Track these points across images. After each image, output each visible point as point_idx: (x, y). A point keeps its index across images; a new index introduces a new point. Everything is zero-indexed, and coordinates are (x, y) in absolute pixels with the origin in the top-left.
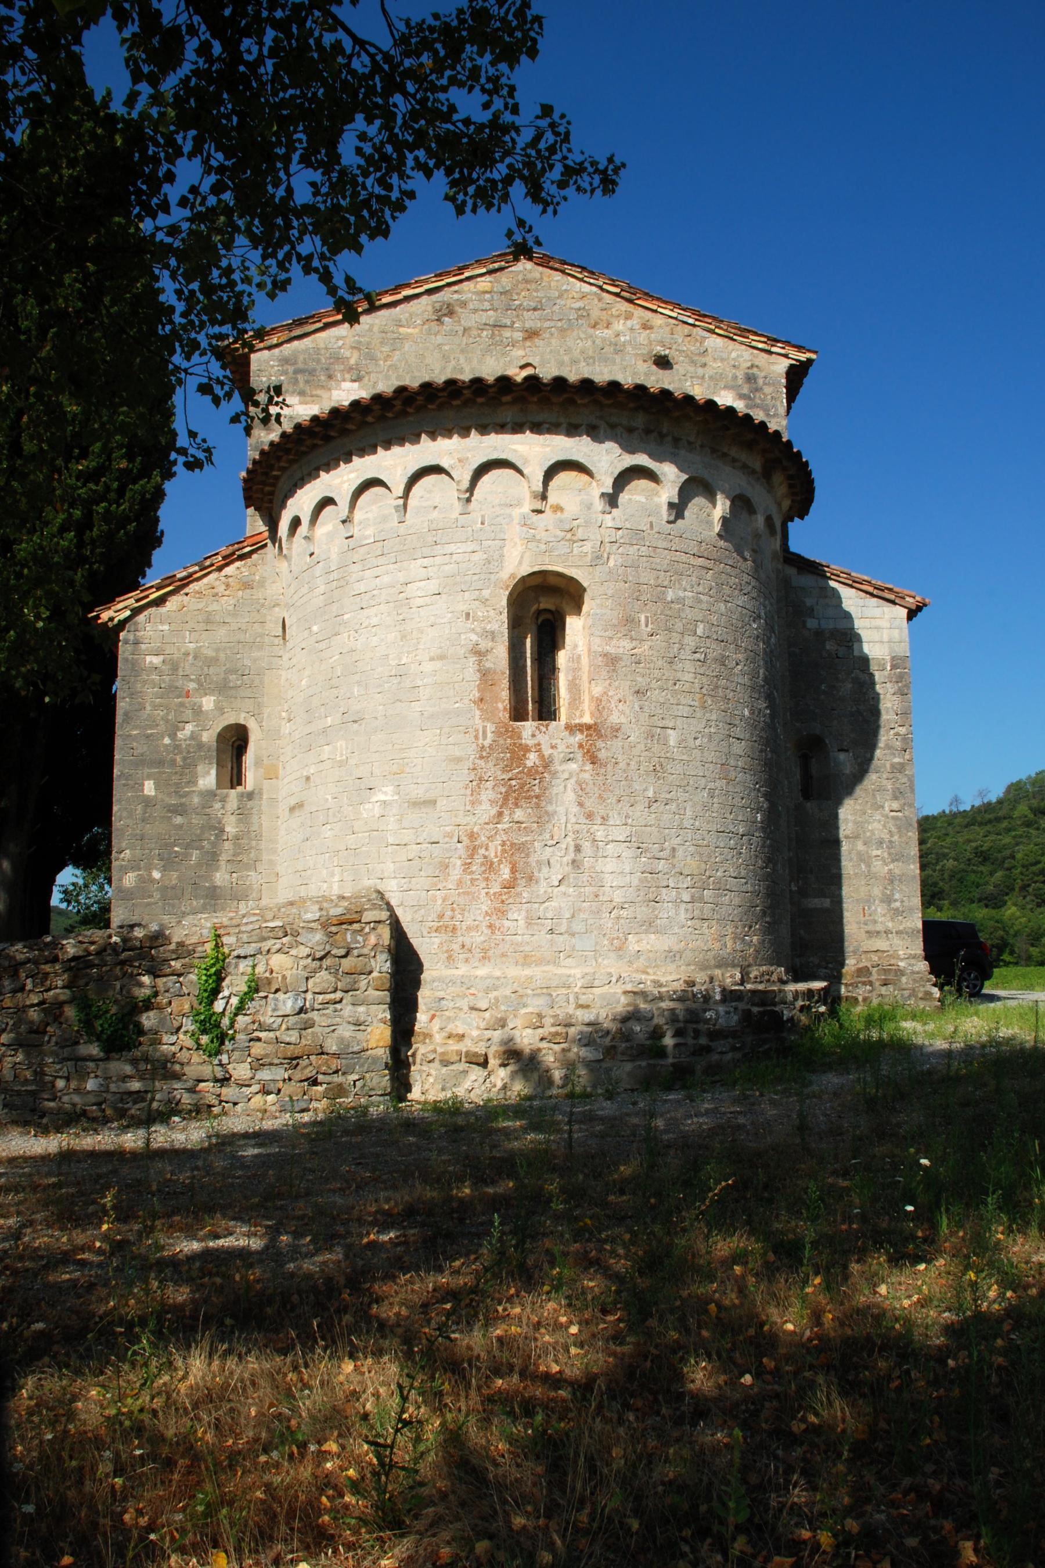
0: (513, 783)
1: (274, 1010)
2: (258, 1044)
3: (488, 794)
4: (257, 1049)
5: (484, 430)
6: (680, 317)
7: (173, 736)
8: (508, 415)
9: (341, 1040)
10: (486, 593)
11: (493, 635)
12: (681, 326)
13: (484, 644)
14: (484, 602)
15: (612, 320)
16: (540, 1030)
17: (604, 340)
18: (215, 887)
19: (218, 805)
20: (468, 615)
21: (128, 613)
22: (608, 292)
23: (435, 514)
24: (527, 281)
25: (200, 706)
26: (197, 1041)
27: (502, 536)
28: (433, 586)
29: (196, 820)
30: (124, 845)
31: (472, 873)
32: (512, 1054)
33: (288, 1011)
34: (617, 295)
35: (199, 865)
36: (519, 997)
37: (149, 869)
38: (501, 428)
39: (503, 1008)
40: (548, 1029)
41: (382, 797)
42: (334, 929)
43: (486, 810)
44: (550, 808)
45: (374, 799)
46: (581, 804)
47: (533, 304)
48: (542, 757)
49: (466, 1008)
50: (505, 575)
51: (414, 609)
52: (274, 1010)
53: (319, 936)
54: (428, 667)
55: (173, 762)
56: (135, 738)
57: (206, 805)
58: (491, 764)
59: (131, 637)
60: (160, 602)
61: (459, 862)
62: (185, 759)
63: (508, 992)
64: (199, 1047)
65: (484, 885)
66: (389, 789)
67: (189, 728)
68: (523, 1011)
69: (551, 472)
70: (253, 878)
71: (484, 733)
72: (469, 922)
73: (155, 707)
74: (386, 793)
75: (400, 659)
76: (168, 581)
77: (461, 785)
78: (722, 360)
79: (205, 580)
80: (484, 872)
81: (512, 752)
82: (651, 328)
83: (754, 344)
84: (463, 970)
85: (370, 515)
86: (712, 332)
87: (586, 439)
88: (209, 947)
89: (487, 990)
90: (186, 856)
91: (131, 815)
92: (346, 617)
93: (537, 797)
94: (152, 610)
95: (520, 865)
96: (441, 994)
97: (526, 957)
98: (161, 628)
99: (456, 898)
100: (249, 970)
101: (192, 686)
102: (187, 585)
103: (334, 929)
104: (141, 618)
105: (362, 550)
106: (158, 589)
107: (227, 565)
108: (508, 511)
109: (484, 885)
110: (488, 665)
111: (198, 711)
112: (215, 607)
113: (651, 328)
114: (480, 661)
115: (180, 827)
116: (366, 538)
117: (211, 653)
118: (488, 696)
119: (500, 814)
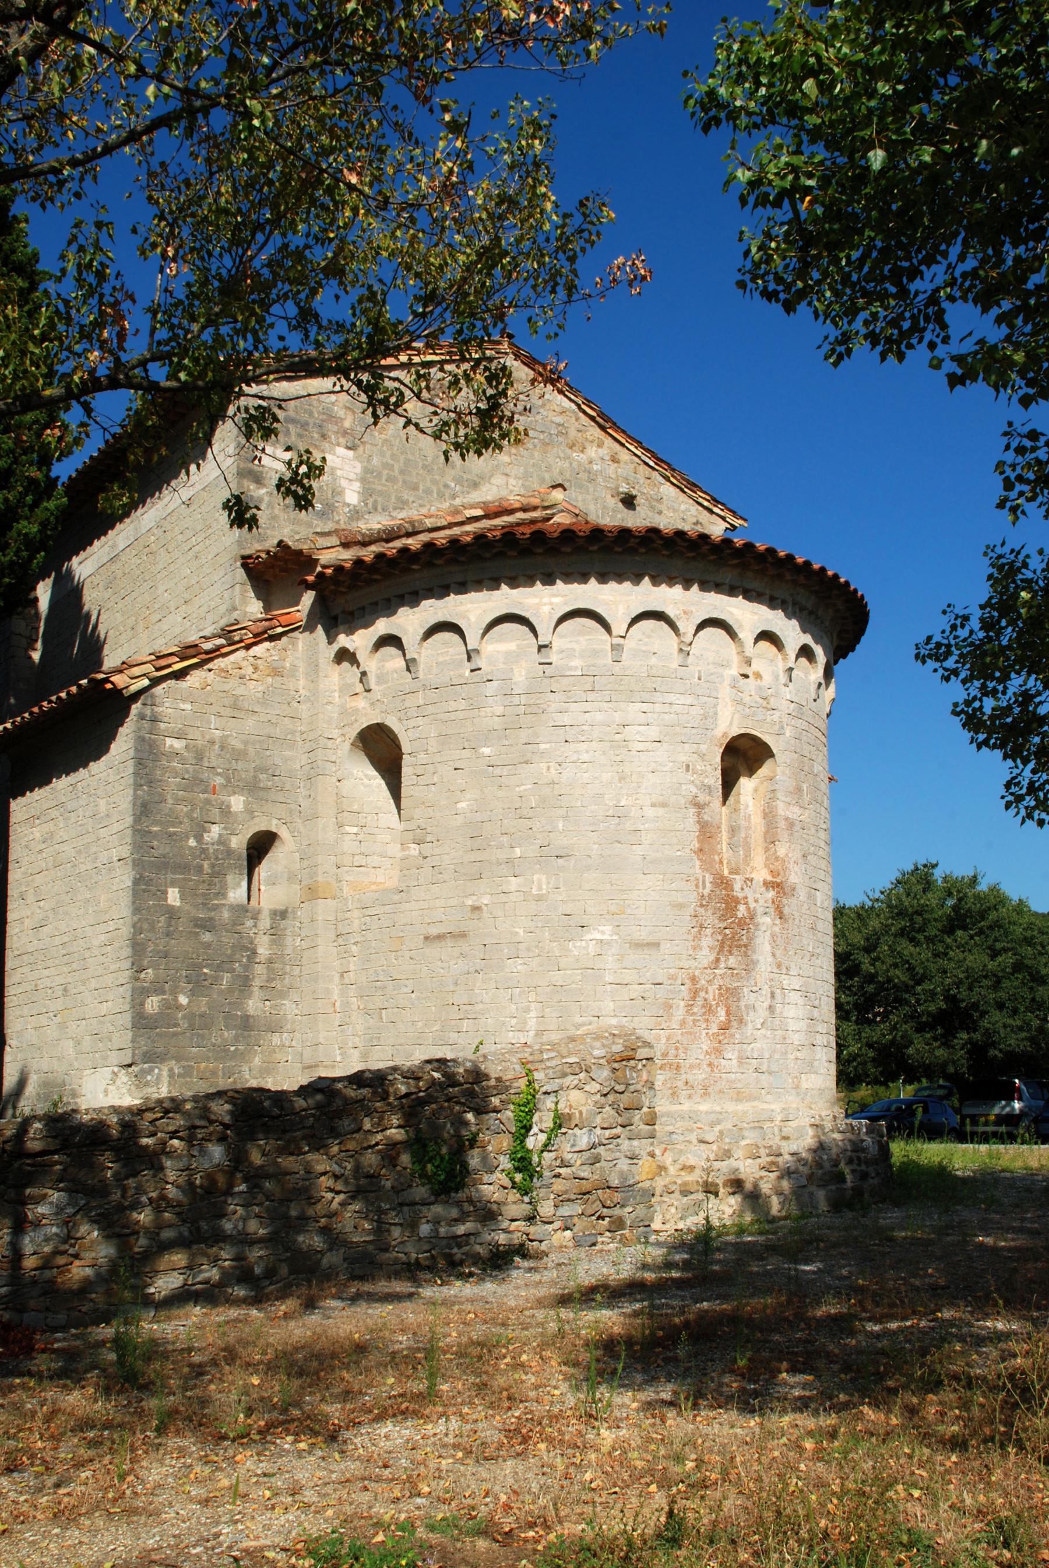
0: (727, 931)
1: (573, 1146)
2: (559, 1180)
4: (559, 1185)
5: (705, 587)
6: (644, 458)
7: (199, 838)
8: (728, 576)
9: (621, 1172)
10: (703, 748)
11: (709, 789)
12: (643, 467)
13: (703, 798)
14: (702, 756)
15: (587, 445)
16: (759, 1160)
17: (580, 464)
18: (248, 1016)
19: (249, 923)
20: (688, 766)
21: (146, 682)
22: (584, 412)
23: (653, 661)
25: (229, 806)
26: (512, 1180)
27: (714, 694)
28: (653, 733)
29: (228, 939)
30: (145, 963)
31: (694, 1014)
32: (737, 1185)
33: (584, 1147)
34: (592, 418)
35: (230, 990)
36: (739, 1132)
37: (174, 993)
38: (718, 587)
39: (727, 1140)
40: (765, 1160)
41: (599, 936)
42: (616, 1065)
43: (706, 956)
44: (755, 957)
45: (588, 937)
46: (774, 955)
48: (748, 909)
49: (695, 1141)
50: (719, 732)
51: (634, 753)
52: (573, 1146)
53: (606, 1073)
54: (650, 812)
55: (200, 869)
56: (155, 835)
57: (237, 922)
58: (710, 912)
59: (148, 712)
61: (682, 1004)
62: (213, 866)
63: (729, 1126)
64: (514, 1185)
65: (704, 1025)
66: (608, 929)
67: (215, 830)
68: (743, 1143)
70: (289, 1007)
71: (704, 882)
72: (691, 1061)
73: (178, 801)
74: (603, 933)
75: (619, 801)
76: (192, 651)
77: (684, 930)
78: (674, 511)
79: (232, 658)
80: (704, 1014)
81: (727, 902)
82: (618, 462)
83: (700, 500)
84: (686, 1106)
85: (575, 646)
86: (667, 479)
87: (780, 613)
88: (522, 1083)
89: (712, 1125)
90: (217, 979)
92: (542, 746)
93: (746, 946)
94: (172, 683)
95: (733, 1008)
96: (671, 1128)
97: (738, 1093)
98: (182, 706)
99: (679, 1038)
100: (553, 1106)
101: (219, 781)
102: (211, 660)
103: (616, 1065)
104: (158, 690)
105: (565, 681)
106: (182, 659)
107: (255, 644)
108: (720, 670)
109: (704, 1025)
110: (706, 818)
111: (226, 811)
112: (240, 691)
113: (618, 462)
114: (699, 813)
115: (208, 945)
116: (571, 669)
117: (237, 744)
118: (706, 848)
119: (718, 960)
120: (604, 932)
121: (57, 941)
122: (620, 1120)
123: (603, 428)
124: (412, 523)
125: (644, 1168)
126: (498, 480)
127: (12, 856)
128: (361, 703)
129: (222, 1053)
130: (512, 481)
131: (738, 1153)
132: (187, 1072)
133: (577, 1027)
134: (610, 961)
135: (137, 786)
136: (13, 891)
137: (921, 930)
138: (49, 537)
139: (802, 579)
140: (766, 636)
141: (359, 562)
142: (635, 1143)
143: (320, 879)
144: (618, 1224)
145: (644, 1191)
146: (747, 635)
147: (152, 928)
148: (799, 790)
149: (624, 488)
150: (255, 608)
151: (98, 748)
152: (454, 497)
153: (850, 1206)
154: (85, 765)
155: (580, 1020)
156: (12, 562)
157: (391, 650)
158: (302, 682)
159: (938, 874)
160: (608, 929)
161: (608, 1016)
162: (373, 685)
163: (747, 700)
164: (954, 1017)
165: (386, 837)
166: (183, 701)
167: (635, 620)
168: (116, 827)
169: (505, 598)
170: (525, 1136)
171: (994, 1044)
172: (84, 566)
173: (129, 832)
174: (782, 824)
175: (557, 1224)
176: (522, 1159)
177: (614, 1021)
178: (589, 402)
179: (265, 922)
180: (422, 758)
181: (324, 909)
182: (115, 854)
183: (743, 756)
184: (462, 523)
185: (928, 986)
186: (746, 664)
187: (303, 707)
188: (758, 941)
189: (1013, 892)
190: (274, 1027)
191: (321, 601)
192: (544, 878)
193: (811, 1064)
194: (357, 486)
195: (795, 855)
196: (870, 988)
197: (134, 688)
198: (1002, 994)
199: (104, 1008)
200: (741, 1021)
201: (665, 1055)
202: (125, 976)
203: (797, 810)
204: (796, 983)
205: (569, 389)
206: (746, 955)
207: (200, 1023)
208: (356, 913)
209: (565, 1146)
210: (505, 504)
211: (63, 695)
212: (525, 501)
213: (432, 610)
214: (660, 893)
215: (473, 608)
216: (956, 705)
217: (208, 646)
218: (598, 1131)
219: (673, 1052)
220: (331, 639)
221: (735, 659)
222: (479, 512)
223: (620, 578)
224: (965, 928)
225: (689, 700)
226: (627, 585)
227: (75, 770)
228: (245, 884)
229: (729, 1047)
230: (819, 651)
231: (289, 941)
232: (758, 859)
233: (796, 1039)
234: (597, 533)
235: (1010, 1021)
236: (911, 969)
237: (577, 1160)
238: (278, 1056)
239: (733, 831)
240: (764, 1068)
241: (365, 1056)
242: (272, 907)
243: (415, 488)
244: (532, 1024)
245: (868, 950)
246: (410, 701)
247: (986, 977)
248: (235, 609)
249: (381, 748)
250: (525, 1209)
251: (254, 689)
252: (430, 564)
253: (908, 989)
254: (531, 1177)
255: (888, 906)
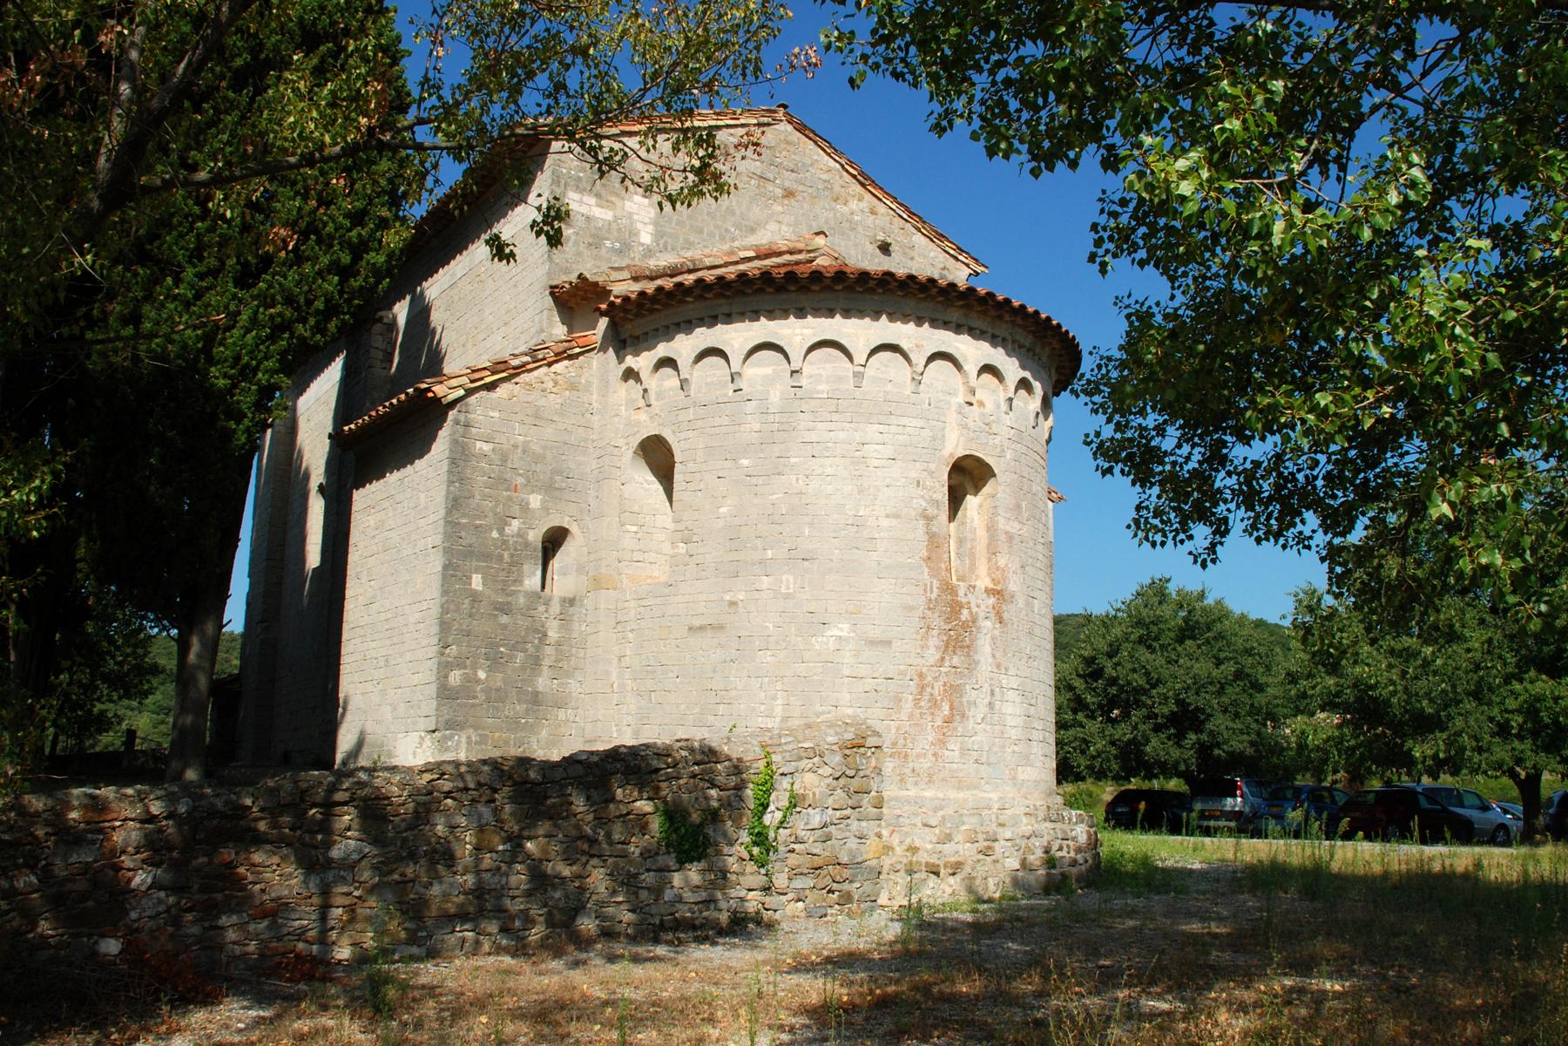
3: (934, 641)
4: (793, 860)
7: (501, 531)
8: (955, 315)
9: (851, 850)
10: (932, 466)
11: (937, 503)
13: (931, 511)
14: (931, 473)
19: (542, 608)
21: (462, 392)
23: (889, 387)
24: (788, 143)
26: (750, 852)
28: (888, 451)
29: (522, 622)
34: (854, 177)
35: (523, 668)
37: (475, 669)
41: (838, 633)
43: (932, 655)
45: (829, 633)
47: (792, 166)
50: (946, 452)
53: (838, 758)
54: (885, 522)
56: (464, 527)
57: (531, 607)
59: (462, 417)
60: (491, 387)
62: (512, 556)
66: (846, 626)
67: (516, 524)
69: (933, 357)
70: (573, 686)
72: (918, 750)
73: (485, 497)
76: (502, 367)
87: (1001, 350)
88: (761, 764)
89: (935, 810)
90: (511, 657)
91: (457, 610)
94: (484, 393)
95: (956, 704)
96: (898, 812)
101: (520, 480)
102: (518, 375)
104: (472, 399)
105: (813, 403)
106: (493, 373)
111: (525, 508)
112: (542, 402)
115: (504, 627)
116: (819, 392)
119: (943, 659)
120: (842, 629)
121: (383, 617)
122: (850, 802)
123: (863, 185)
124: (693, 261)
125: (870, 849)
126: (773, 226)
127: (352, 541)
128: (643, 416)
129: (514, 724)
130: (784, 228)
131: (958, 837)
132: (483, 740)
133: (818, 715)
134: (847, 657)
135: (450, 483)
136: (351, 571)
137: (1156, 639)
138: (394, 267)
139: (1019, 320)
140: (988, 369)
141: (642, 294)
142: (864, 824)
143: (603, 571)
144: (847, 898)
145: (872, 869)
146: (971, 368)
147: (457, 610)
148: (1018, 507)
149: (881, 237)
150: (560, 331)
151: (423, 449)
152: (733, 240)
153: (1058, 890)
154: (412, 463)
155: (820, 709)
156: (361, 287)
157: (668, 371)
158: (595, 397)
159: (1172, 588)
160: (846, 626)
161: (845, 704)
162: (653, 402)
163: (971, 424)
164: (1185, 719)
165: (661, 536)
166: (493, 409)
167: (874, 351)
168: (432, 518)
169: (763, 329)
170: (763, 813)
171: (1218, 745)
172: (434, 288)
173: (442, 523)
174: (1003, 537)
175: (790, 896)
176: (759, 834)
177: (850, 711)
178: (851, 163)
179: (555, 608)
180: (691, 466)
181: (605, 599)
182: (430, 542)
183: (968, 476)
184: (737, 263)
185: (1161, 690)
186: (974, 395)
187: (595, 418)
188: (980, 642)
189: (1236, 606)
190: (560, 705)
191: (613, 326)
192: (791, 579)
193: (1027, 757)
194: (650, 228)
195: (1014, 566)
196: (1113, 690)
197: (451, 398)
198: (1225, 699)
199: (416, 679)
200: (963, 716)
201: (894, 744)
202: (433, 651)
203: (1016, 525)
204: (1014, 683)
205: (832, 149)
206: (968, 655)
207: (496, 697)
208: (633, 604)
209: (799, 824)
210: (774, 248)
211: (394, 401)
212: (791, 245)
213: (704, 336)
214: (892, 597)
215: (737, 336)
216: (1087, 436)
217: (515, 362)
218: (830, 811)
219: (901, 741)
220: (621, 360)
221: (961, 389)
222: (752, 254)
223: (861, 314)
224: (1194, 638)
225: (920, 423)
226: (867, 320)
227: (404, 466)
228: (539, 573)
229: (952, 739)
230: (1037, 386)
231: (576, 625)
232: (982, 569)
233: (1014, 734)
234: (864, 276)
235: (1230, 724)
236: (1147, 674)
237: (810, 837)
238: (563, 730)
239: (961, 542)
240: (984, 760)
241: (636, 734)
242: (563, 594)
243: (701, 231)
244: (779, 710)
245: (1110, 655)
246: (683, 416)
247: (1211, 683)
248: (543, 331)
249: (658, 456)
250: (761, 880)
251: (553, 401)
252: (701, 297)
253: (1145, 692)
254: (768, 851)
255: (1130, 616)
